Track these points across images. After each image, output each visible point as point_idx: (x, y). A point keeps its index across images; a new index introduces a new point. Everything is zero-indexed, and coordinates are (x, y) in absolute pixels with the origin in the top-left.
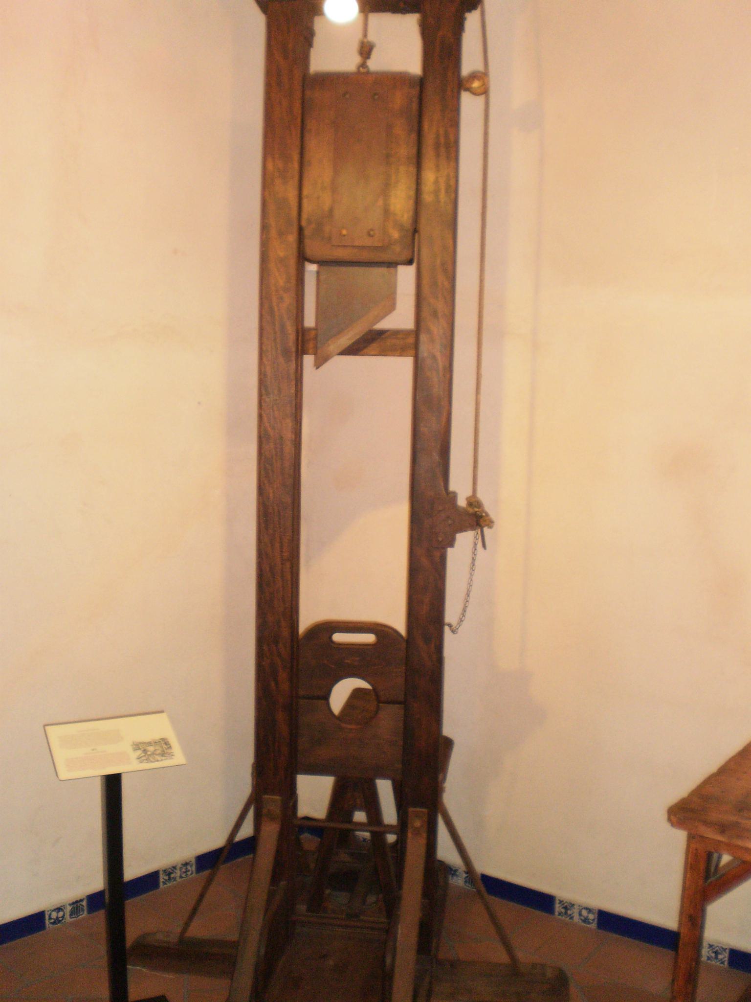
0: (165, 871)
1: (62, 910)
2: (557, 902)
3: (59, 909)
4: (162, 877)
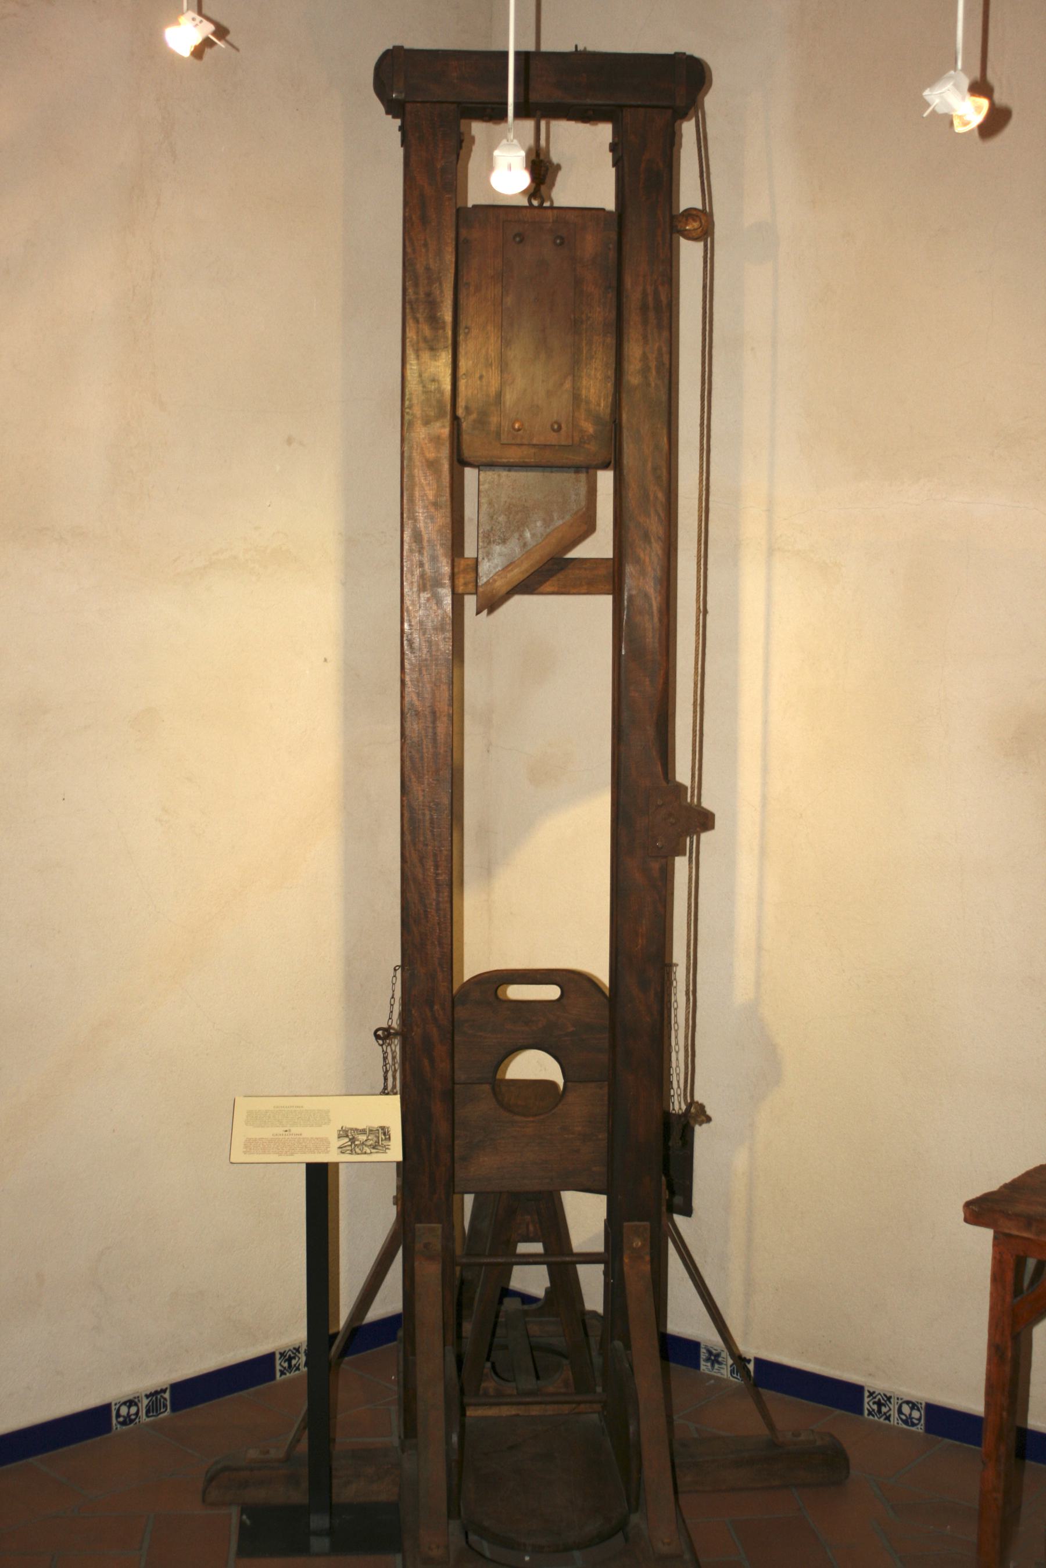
0: (282, 1354)
1: (136, 1405)
2: (866, 1394)
3: (130, 1403)
4: (279, 1364)
